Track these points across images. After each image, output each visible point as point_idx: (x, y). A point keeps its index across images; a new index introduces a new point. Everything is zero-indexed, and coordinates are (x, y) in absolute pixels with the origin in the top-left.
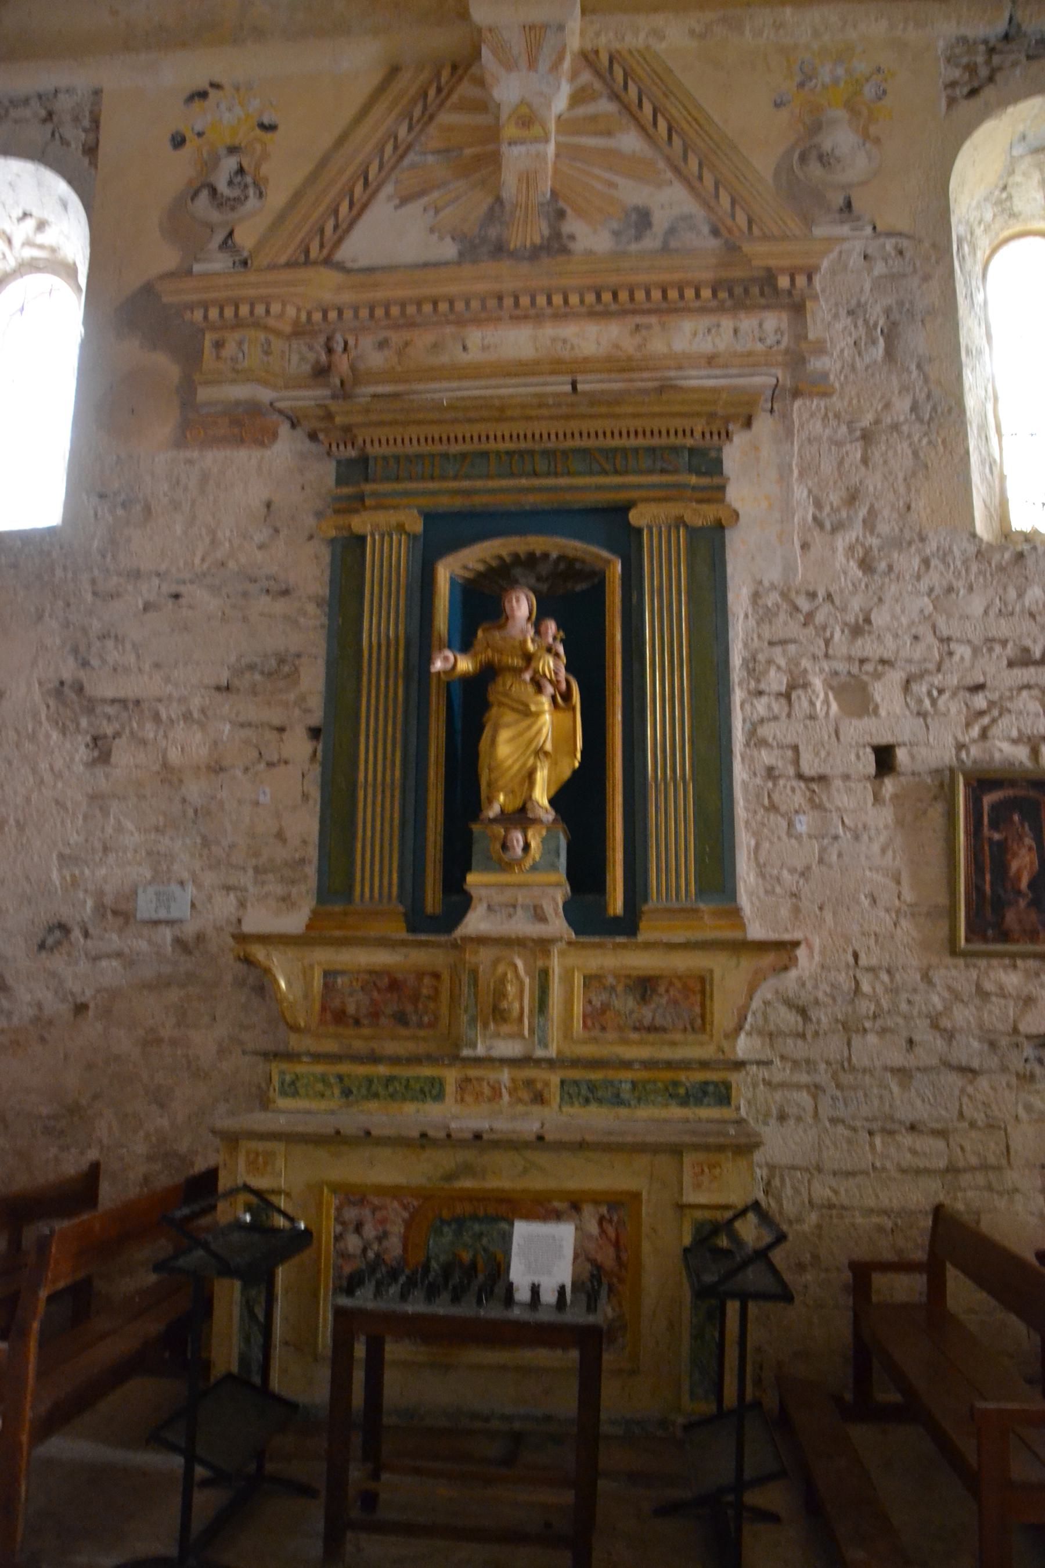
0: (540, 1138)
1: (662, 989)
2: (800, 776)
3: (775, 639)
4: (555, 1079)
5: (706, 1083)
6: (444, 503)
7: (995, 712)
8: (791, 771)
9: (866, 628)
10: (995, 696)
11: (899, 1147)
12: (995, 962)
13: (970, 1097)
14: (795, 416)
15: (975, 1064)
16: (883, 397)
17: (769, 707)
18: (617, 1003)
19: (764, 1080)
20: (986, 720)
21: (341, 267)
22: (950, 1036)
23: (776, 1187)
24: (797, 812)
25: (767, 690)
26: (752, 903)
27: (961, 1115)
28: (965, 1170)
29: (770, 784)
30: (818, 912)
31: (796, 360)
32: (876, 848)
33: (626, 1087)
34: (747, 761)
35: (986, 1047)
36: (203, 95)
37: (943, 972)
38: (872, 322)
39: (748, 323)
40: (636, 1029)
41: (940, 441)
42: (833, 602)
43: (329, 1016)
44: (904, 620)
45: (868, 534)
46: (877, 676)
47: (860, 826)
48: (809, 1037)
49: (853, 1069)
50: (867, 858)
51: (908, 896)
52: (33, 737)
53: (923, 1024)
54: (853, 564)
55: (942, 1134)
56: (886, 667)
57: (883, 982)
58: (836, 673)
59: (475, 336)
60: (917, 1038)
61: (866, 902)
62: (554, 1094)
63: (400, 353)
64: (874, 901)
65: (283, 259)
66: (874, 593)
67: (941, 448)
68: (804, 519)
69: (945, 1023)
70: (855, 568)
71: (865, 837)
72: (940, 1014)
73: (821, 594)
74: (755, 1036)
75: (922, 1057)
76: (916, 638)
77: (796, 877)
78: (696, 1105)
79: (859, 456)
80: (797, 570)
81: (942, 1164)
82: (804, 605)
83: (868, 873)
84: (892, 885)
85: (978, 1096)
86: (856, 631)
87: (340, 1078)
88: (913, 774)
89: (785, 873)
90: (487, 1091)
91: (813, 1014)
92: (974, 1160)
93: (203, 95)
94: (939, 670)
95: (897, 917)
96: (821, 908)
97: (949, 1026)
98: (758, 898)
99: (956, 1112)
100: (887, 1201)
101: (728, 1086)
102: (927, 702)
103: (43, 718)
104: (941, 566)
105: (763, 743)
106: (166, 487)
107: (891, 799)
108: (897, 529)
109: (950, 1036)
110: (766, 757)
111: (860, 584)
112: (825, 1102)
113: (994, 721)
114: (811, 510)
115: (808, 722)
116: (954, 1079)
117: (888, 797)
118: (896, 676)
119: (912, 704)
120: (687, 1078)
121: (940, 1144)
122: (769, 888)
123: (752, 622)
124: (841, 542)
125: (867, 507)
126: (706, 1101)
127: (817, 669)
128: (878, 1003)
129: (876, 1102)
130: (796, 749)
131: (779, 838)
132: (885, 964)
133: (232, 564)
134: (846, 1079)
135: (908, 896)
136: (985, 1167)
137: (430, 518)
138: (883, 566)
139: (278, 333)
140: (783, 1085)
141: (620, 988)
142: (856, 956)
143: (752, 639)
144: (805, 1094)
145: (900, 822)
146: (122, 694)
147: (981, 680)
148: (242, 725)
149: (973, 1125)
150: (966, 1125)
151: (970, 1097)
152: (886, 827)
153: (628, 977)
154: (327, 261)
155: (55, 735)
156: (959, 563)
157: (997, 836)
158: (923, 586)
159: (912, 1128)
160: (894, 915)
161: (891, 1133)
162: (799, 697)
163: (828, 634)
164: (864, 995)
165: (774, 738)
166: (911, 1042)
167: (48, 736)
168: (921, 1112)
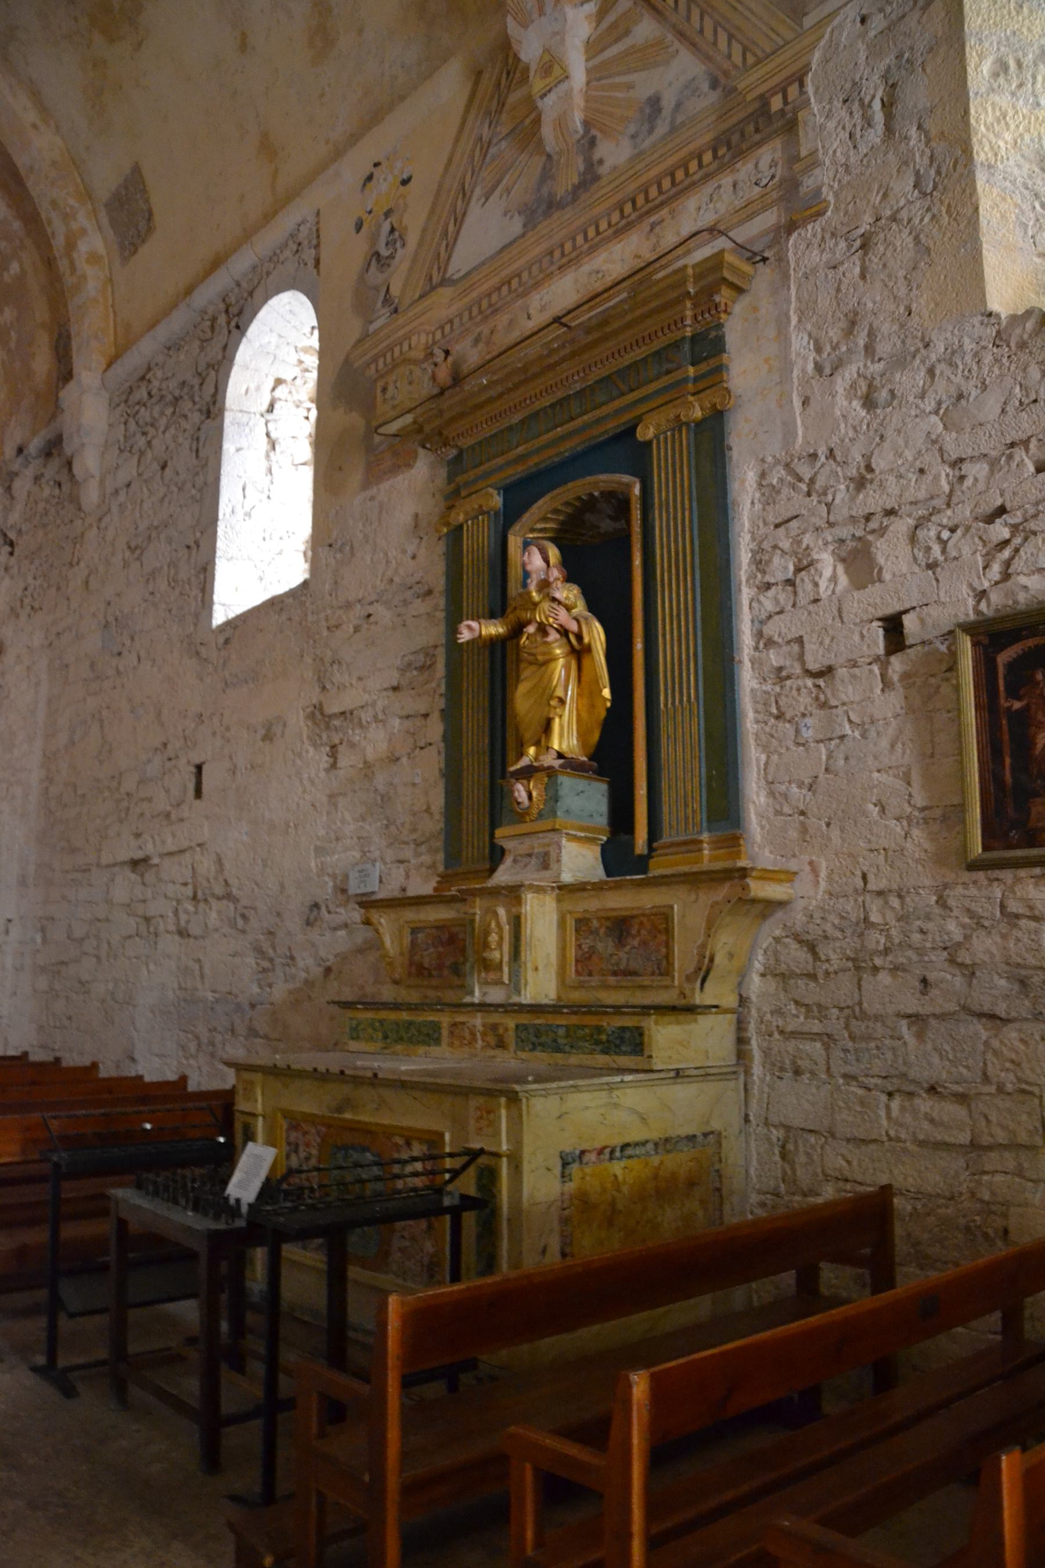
0: (466, 1095)
1: (634, 932)
2: (809, 673)
3: (779, 520)
4: (511, 1022)
5: (623, 1029)
6: (518, 471)
7: (1017, 541)
8: (798, 670)
9: (869, 476)
10: (1017, 518)
11: (915, 1112)
12: (1022, 873)
13: (996, 1053)
14: (790, 254)
15: (1001, 1009)
16: (880, 186)
17: (776, 600)
18: (600, 946)
19: (778, 1027)
20: (1007, 553)
21: (451, 282)
22: (970, 972)
23: (790, 1151)
24: (804, 715)
25: (772, 581)
26: (762, 827)
27: (986, 1079)
28: (990, 1148)
29: (777, 689)
30: (824, 827)
31: (790, 186)
32: (884, 743)
33: (561, 1032)
34: (756, 665)
35: (1016, 987)
36: (370, 178)
37: (960, 890)
38: (866, 101)
39: (745, 170)
40: (615, 974)
41: (944, 210)
42: (835, 460)
43: (413, 970)
44: (909, 455)
45: (869, 364)
46: (882, 531)
47: (867, 720)
48: (820, 975)
49: (864, 1016)
50: (875, 758)
51: (919, 801)
52: (300, 755)
53: (939, 958)
54: (856, 404)
55: (962, 1098)
56: (892, 518)
57: (893, 908)
58: (842, 541)
59: (535, 301)
60: (932, 976)
61: (875, 811)
62: (510, 1037)
63: (488, 343)
64: (883, 810)
65: (417, 296)
66: (876, 431)
67: (946, 219)
68: (804, 371)
69: (964, 957)
70: (858, 408)
71: (872, 733)
72: (959, 945)
73: (822, 452)
74: (769, 977)
75: (938, 1002)
76: (922, 471)
77: (804, 791)
78: (616, 1053)
79: (857, 270)
80: (796, 433)
81: (965, 1138)
82: (806, 472)
83: (876, 775)
84: (899, 784)
85: (1005, 1051)
86: (860, 483)
87: (381, 1022)
88: (923, 643)
89: (794, 789)
90: (467, 1034)
91: (823, 951)
92: (1001, 1137)
93: (370, 178)
94: (948, 505)
95: (909, 825)
96: (828, 825)
97: (968, 961)
98: (768, 819)
99: (980, 1073)
100: (901, 1179)
101: (639, 1032)
102: (936, 549)
103: (305, 736)
104: (948, 372)
105: (770, 643)
106: (360, 525)
107: (901, 680)
108: (899, 343)
109: (970, 972)
110: (774, 658)
111: (861, 427)
112: (837, 1054)
113: (1017, 550)
114: (812, 355)
115: (811, 607)
116: (981, 1030)
117: (896, 678)
118: (901, 526)
119: (920, 555)
120: (609, 1024)
121: (959, 1112)
122: (778, 808)
123: (758, 506)
124: (841, 384)
125: (866, 332)
126: (624, 1048)
127: (820, 542)
128: (888, 937)
129: (889, 1055)
130: (800, 640)
131: (788, 749)
132: (895, 887)
133: (397, 579)
134: (859, 1027)
135: (919, 801)
136: (1014, 1146)
137: (507, 490)
138: (884, 394)
139: (415, 362)
140: (795, 1034)
141: (602, 931)
142: (864, 877)
143: (759, 527)
144: (818, 1045)
145: (910, 709)
146: (342, 709)
147: (999, 502)
148: (408, 717)
149: (1001, 1089)
150: (992, 1089)
151: (996, 1053)
152: (896, 716)
153: (608, 919)
154: (444, 282)
155: (311, 750)
156: (968, 358)
157: (1017, 705)
158: (929, 405)
159: (932, 1090)
160: (905, 823)
161: (911, 1094)
162: (802, 580)
163: (830, 498)
164: (873, 925)
165: (780, 635)
166: (924, 981)
167: (307, 751)
168: (938, 1070)
